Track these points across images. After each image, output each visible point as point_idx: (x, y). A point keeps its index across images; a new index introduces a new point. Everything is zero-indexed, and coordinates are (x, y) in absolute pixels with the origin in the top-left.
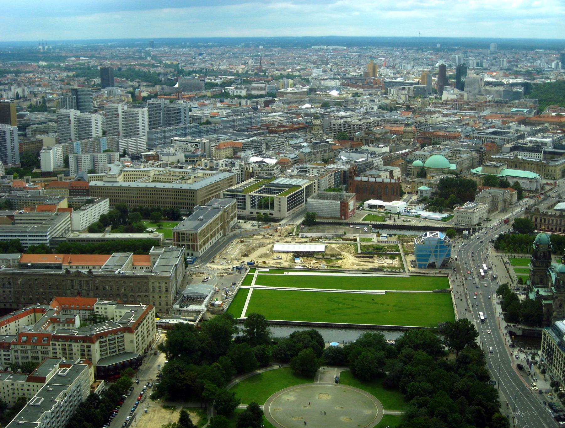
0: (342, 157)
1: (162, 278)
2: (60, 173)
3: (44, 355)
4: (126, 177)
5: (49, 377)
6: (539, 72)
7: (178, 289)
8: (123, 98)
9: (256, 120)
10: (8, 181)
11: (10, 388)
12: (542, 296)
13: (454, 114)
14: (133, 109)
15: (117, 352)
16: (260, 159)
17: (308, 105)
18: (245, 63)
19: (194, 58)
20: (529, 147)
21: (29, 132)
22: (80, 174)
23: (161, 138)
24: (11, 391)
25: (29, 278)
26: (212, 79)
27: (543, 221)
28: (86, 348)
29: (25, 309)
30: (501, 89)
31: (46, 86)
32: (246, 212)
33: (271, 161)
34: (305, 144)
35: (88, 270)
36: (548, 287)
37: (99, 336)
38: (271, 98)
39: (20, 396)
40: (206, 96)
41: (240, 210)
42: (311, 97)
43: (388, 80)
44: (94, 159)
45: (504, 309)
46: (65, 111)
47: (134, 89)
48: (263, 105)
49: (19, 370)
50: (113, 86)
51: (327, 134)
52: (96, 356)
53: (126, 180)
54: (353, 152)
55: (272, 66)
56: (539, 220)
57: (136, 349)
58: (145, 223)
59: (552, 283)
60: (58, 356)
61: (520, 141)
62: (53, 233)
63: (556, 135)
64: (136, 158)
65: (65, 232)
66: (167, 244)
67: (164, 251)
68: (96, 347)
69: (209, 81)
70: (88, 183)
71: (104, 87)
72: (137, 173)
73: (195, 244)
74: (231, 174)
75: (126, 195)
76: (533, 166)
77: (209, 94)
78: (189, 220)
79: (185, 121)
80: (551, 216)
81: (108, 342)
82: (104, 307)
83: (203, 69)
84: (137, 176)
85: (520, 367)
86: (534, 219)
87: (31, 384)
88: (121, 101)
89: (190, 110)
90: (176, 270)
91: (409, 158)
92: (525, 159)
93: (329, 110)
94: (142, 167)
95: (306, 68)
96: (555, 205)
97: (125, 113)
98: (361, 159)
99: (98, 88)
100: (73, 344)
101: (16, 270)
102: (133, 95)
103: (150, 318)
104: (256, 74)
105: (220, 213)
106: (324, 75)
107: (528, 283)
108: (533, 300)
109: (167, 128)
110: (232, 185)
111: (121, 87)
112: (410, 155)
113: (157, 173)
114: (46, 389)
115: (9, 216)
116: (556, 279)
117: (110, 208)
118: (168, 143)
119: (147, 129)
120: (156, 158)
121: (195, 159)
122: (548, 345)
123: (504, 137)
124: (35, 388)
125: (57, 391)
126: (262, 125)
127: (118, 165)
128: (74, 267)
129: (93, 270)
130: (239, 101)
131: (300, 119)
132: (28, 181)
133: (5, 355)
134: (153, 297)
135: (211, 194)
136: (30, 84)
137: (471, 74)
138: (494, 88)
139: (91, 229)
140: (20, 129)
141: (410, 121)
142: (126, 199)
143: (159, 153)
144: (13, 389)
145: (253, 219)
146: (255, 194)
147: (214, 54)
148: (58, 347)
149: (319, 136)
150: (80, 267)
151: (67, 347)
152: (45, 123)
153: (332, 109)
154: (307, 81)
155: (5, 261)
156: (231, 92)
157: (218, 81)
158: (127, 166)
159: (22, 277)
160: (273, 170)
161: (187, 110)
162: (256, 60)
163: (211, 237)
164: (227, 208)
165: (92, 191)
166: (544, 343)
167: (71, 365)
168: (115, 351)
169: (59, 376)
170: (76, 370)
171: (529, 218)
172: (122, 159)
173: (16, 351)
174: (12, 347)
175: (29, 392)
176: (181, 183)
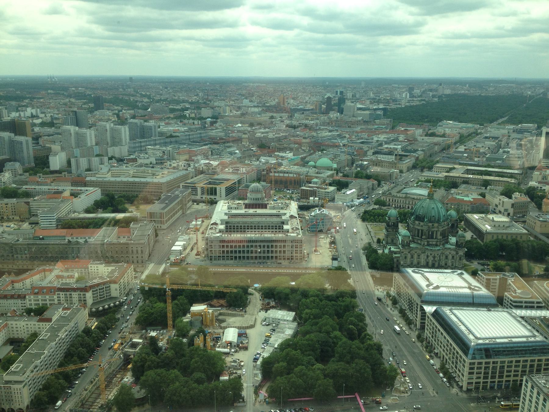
0: (262, 160)
1: (139, 244)
2: (65, 171)
3: (51, 302)
4: (113, 174)
5: (54, 318)
6: (395, 100)
7: (151, 251)
8: (111, 118)
9: (205, 135)
10: (25, 177)
11: (25, 328)
12: (393, 251)
13: (336, 130)
14: (117, 126)
15: (105, 298)
16: (207, 161)
17: (240, 125)
18: (197, 95)
19: (162, 91)
20: (385, 152)
21: (41, 141)
22: (79, 172)
23: (138, 147)
24: (26, 330)
25: (40, 247)
26: (174, 106)
27: (394, 201)
28: (82, 296)
29: (38, 270)
30: (368, 112)
31: (53, 108)
32: (198, 197)
33: (215, 163)
34: (237, 151)
35: (84, 240)
36: (397, 245)
37: (91, 287)
38: (215, 120)
39: (33, 332)
40: (170, 117)
41: (194, 196)
42: (242, 119)
43: (293, 108)
44: (89, 162)
45: (368, 260)
46: (67, 127)
47: (119, 111)
48: (209, 124)
49: (32, 314)
50: (103, 109)
51: (252, 144)
52: (90, 301)
53: (113, 176)
54: (269, 157)
55: (216, 98)
56: (391, 200)
57: (119, 295)
58: (127, 206)
59: (400, 243)
60: (62, 302)
61: (379, 148)
62: (59, 214)
63: (403, 143)
64: (120, 160)
65: (68, 213)
66: (143, 220)
67: (141, 226)
68: (89, 296)
69: (172, 107)
70: (85, 178)
71: (96, 110)
72: (121, 171)
73: (163, 220)
74: (187, 172)
75: (113, 186)
76: (388, 164)
77: (172, 116)
78: (158, 203)
79: (155, 136)
80: (400, 197)
81: (98, 291)
82: (95, 266)
83: (168, 98)
84: (121, 174)
85: (379, 300)
86: (388, 200)
87: (41, 323)
88: (108, 120)
89: (159, 127)
90: (149, 238)
91: (307, 159)
92: (383, 160)
93: (254, 128)
94: (125, 167)
95: (239, 99)
96: (402, 190)
97: (112, 129)
98: (273, 161)
99: (91, 111)
100: (73, 293)
101: (31, 242)
102: (118, 116)
103: (126, 277)
104: (205, 103)
105: (179, 199)
106: (250, 104)
107: (384, 242)
108: (387, 254)
109: (142, 140)
110: (188, 179)
111: (108, 110)
112: (307, 158)
113: (135, 171)
114: (52, 328)
115: (26, 203)
116: (402, 240)
117: (102, 195)
118: (144, 150)
119: (128, 140)
120: (135, 160)
121: (163, 161)
122: (397, 285)
123: (368, 146)
124: (44, 326)
125: (59, 329)
126: (209, 138)
127: (107, 166)
128: (75, 238)
129: (88, 240)
130: (193, 121)
131: (234, 135)
132: (40, 177)
133: (22, 303)
134: (133, 257)
135: (173, 186)
136: (41, 107)
137: (348, 103)
138: (363, 112)
139: (88, 211)
140: (33, 139)
141: (307, 136)
142: (113, 189)
143: (137, 157)
144: (27, 328)
145: (204, 202)
146: (204, 186)
147: (175, 88)
148: (61, 296)
149: (247, 145)
150: (79, 238)
151: (68, 296)
152: (52, 135)
153: (256, 127)
154: (239, 108)
155: (22, 235)
156: (187, 115)
157: (178, 107)
158: (114, 167)
159: (35, 247)
160: (216, 169)
161: (157, 127)
162: (204, 92)
163: (174, 214)
164: (184, 195)
165: (88, 184)
166: (395, 283)
167: (70, 309)
168: (104, 297)
169: (62, 317)
170: (74, 314)
171: (385, 200)
172: (110, 161)
173: (30, 300)
174: (27, 297)
175: (39, 330)
176: (153, 178)
